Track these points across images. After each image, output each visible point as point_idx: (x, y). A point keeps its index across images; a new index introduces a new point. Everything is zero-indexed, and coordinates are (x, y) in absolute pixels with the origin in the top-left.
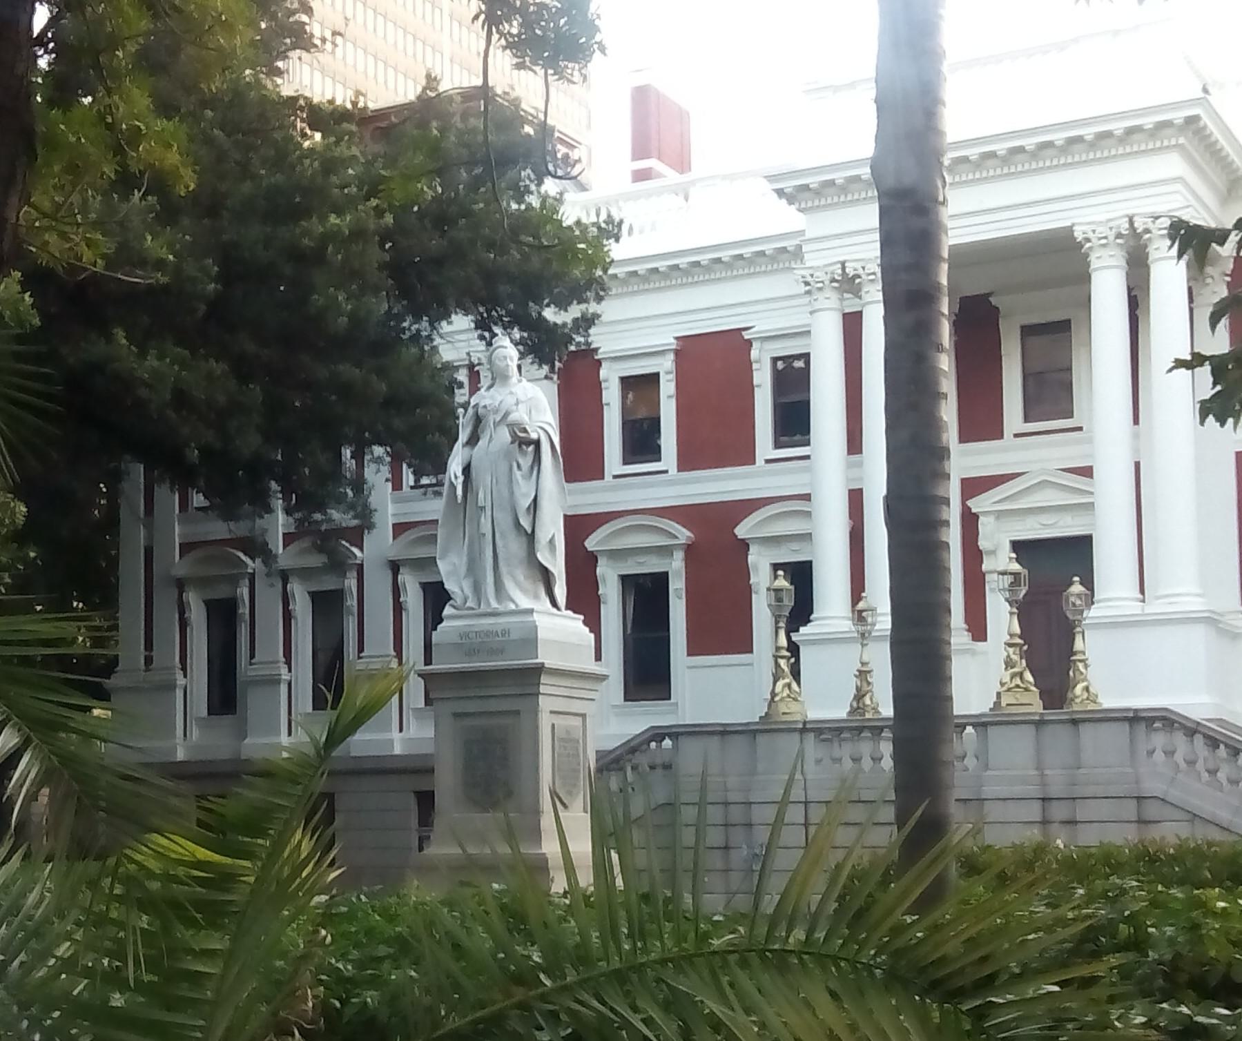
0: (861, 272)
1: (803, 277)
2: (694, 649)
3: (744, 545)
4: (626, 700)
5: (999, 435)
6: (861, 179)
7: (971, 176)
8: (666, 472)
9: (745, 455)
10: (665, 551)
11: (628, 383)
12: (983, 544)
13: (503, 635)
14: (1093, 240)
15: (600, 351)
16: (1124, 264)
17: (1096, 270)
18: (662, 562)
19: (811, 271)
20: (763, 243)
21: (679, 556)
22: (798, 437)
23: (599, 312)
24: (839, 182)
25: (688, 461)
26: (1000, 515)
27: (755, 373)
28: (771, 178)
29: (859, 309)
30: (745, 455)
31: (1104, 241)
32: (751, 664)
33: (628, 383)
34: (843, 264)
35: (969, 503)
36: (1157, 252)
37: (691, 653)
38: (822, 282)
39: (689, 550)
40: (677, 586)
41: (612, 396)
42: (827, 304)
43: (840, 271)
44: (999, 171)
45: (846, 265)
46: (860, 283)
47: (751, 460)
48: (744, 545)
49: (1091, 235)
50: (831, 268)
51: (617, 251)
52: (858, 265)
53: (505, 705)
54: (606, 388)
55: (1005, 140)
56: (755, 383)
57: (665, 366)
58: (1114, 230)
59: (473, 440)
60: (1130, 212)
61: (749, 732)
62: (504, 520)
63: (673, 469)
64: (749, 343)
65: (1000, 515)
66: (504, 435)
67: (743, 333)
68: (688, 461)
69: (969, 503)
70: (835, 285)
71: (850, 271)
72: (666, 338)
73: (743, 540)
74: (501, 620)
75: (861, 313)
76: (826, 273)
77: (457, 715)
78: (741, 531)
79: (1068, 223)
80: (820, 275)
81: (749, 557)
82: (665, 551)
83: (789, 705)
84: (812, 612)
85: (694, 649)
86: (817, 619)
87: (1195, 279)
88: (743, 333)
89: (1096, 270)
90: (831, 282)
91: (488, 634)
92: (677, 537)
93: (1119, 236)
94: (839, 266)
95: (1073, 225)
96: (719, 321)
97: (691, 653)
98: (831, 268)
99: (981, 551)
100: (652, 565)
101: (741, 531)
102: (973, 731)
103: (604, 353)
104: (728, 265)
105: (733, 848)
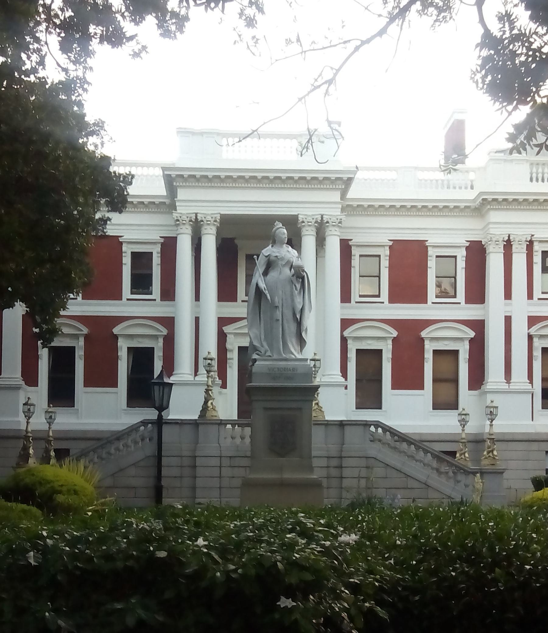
0: (203, 219)
1: (177, 217)
2: (88, 383)
3: (116, 337)
4: (542, 408)
5: (236, 300)
6: (220, 178)
7: (231, 185)
8: (459, 303)
9: (117, 295)
10: (156, 337)
11: (135, 255)
12: (228, 346)
13: (293, 371)
14: (306, 223)
15: (428, 242)
16: (315, 234)
17: (304, 235)
18: (72, 341)
19: (306, 217)
20: (144, 198)
21: (161, 341)
22: (146, 291)
23: (110, 217)
24: (259, 178)
25: (393, 299)
26: (236, 334)
27: (123, 258)
28: (164, 169)
29: (175, 236)
30: (117, 295)
31: (334, 224)
32: (117, 393)
33: (135, 255)
34: (196, 214)
35: (224, 328)
36: (181, 230)
37: (393, 388)
38: (185, 221)
39: (87, 338)
40: (80, 353)
41: (127, 260)
42: (211, 232)
43: (194, 218)
44: (267, 186)
45: (324, 216)
46: (202, 224)
47: (426, 302)
48: (116, 337)
49: (305, 220)
50: (215, 215)
51: (132, 190)
52: (203, 216)
53: (294, 405)
54: (125, 256)
55: (225, 171)
56: (123, 262)
57: (461, 254)
58: (188, 219)
59: (265, 273)
60: (322, 213)
61: (195, 424)
62: (288, 314)
63: (463, 300)
64: (121, 243)
65: (236, 334)
66: (287, 272)
67: (119, 238)
68: (393, 299)
69: (224, 328)
70: (191, 223)
71: (199, 218)
72: (385, 239)
73: (116, 335)
74: (289, 363)
75: (176, 237)
76: (337, 219)
77: (266, 409)
78: (116, 331)
79: (296, 214)
80: (184, 217)
81: (119, 343)
82: (76, 337)
83: (317, 413)
84: (173, 371)
85: (88, 383)
86: (199, 374)
87: (319, 246)
88: (119, 238)
89: (304, 235)
90: (315, 223)
91: (285, 369)
92: (82, 331)
93: (191, 221)
94: (195, 215)
95: (298, 214)
96: (403, 235)
97: (393, 388)
98: (215, 215)
99: (227, 349)
100: (146, 344)
101: (116, 331)
102: (231, 427)
103: (353, 243)
104: (398, 209)
105: (345, 478)
